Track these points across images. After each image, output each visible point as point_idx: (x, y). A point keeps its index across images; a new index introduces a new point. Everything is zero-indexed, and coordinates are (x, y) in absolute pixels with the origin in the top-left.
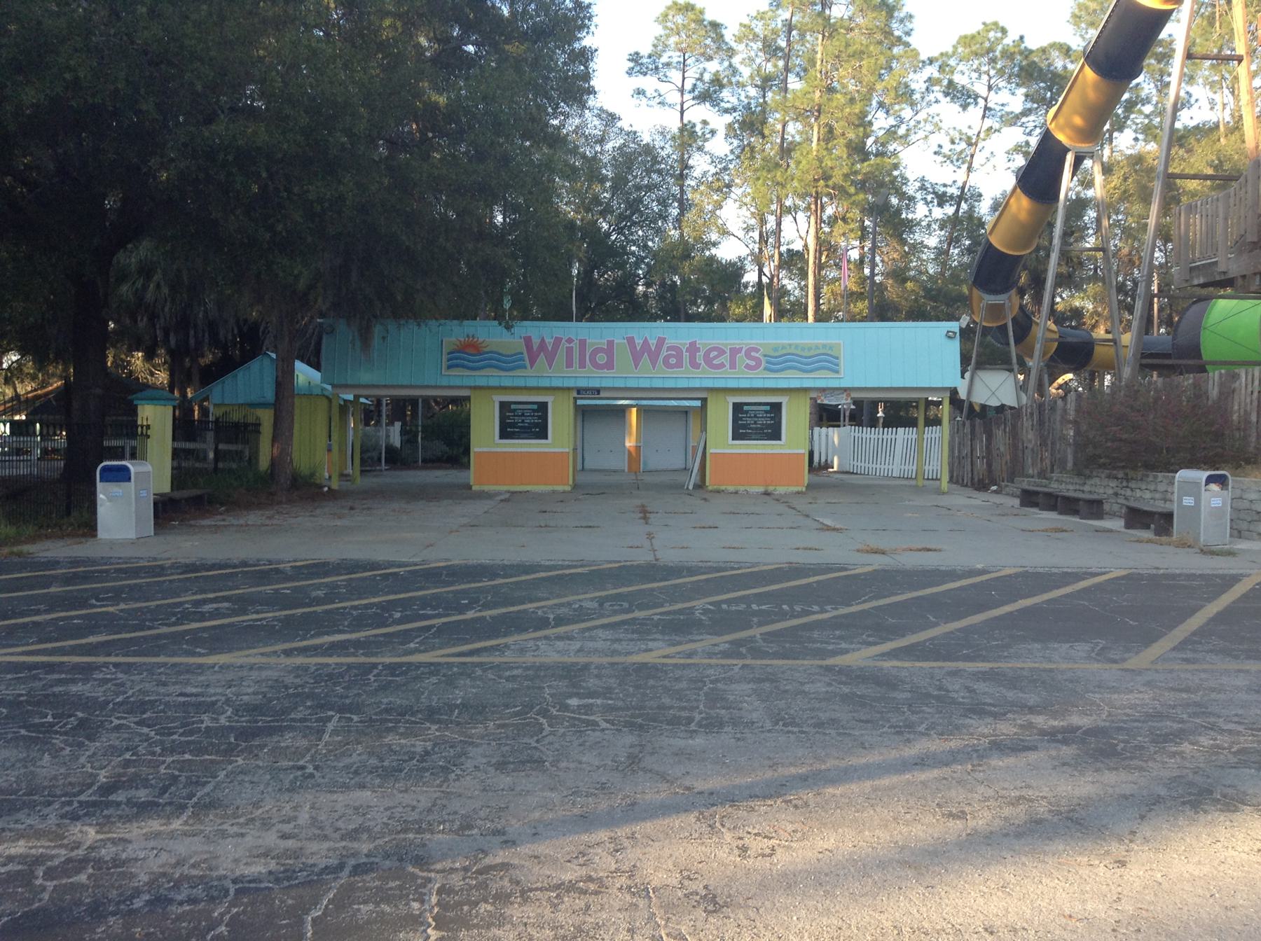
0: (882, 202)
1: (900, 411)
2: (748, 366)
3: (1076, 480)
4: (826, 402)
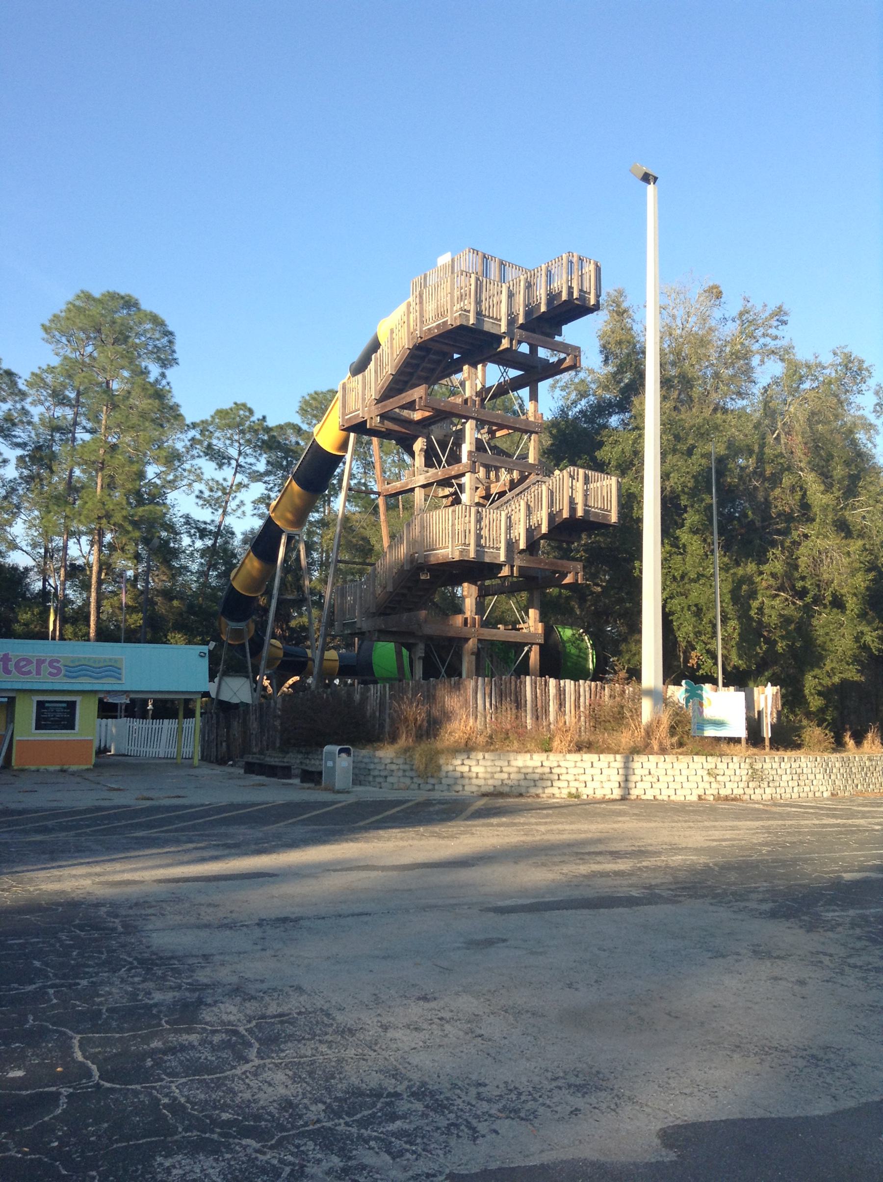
0: (154, 536)
1: (168, 708)
2: (51, 674)
3: (280, 755)
4: (111, 701)
